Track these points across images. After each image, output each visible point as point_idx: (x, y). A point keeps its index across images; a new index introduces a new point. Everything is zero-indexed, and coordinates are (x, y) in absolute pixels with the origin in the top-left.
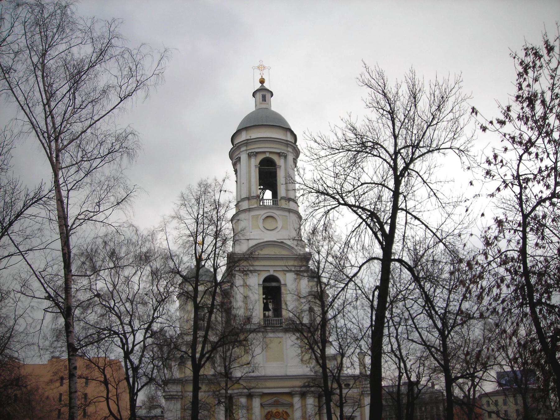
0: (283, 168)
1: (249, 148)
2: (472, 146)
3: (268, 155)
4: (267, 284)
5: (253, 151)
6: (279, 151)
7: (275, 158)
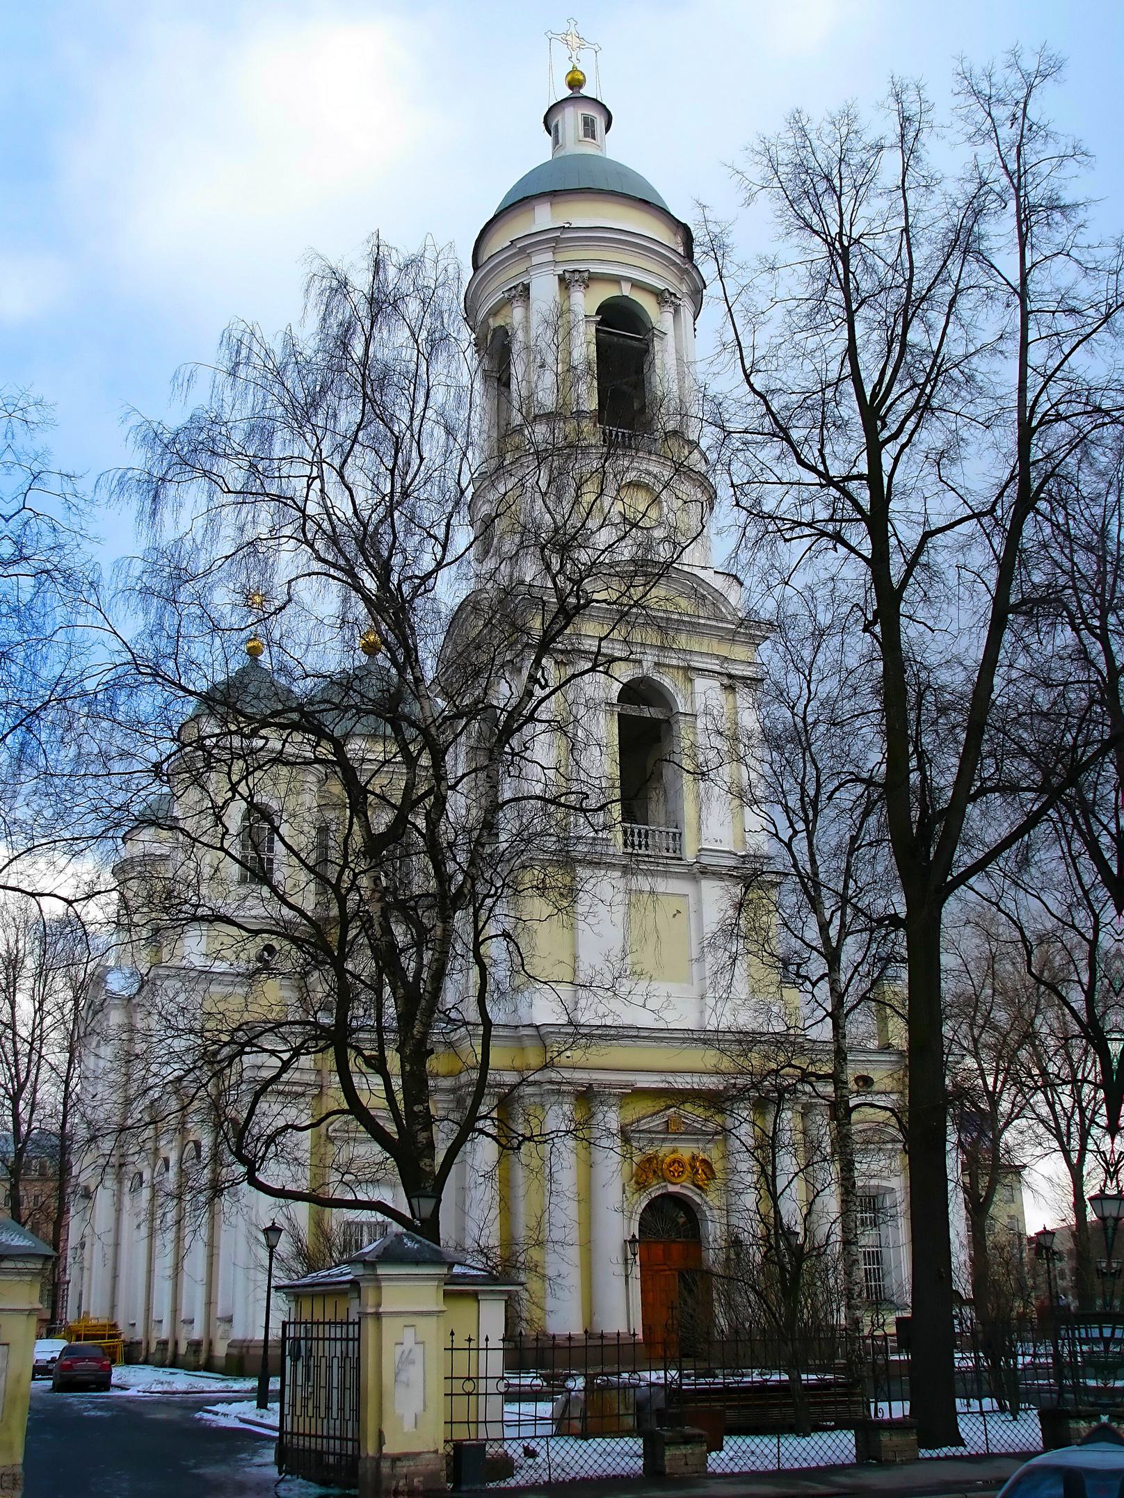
0: (670, 339)
1: (559, 258)
2: (487, 1340)
3: (626, 290)
4: (632, 710)
5: (582, 267)
6: (661, 286)
7: (648, 303)
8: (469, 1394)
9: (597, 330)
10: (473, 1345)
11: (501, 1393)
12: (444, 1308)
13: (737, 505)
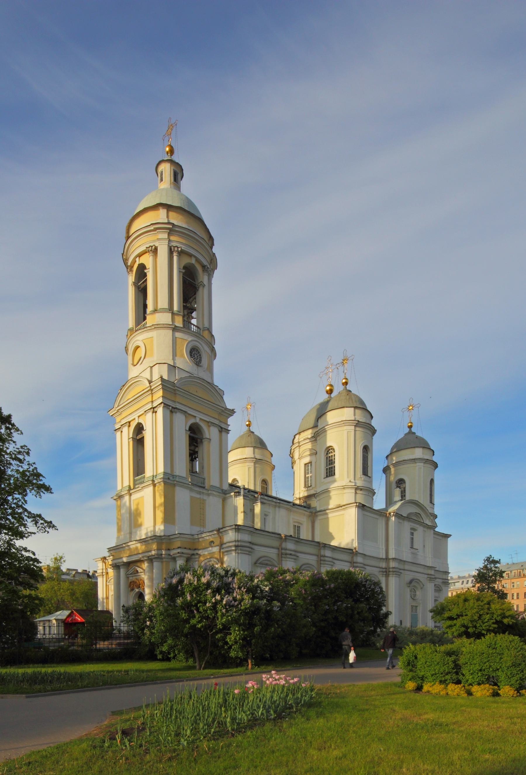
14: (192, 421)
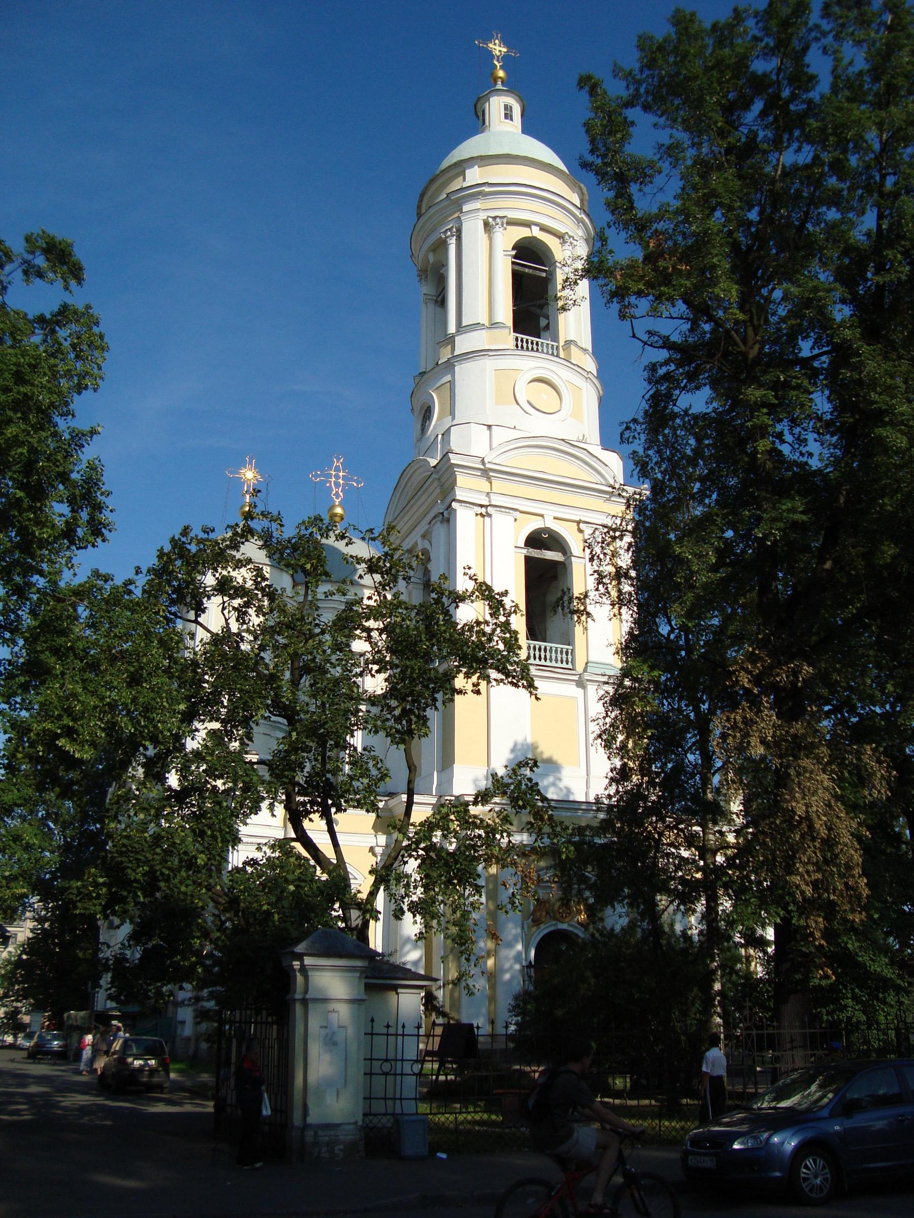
2: (403, 1026)
3: (536, 232)
8: (386, 1074)
9: (513, 263)
10: (392, 1031)
11: (414, 1074)
12: (365, 997)
13: (634, 336)
14: (535, 524)
